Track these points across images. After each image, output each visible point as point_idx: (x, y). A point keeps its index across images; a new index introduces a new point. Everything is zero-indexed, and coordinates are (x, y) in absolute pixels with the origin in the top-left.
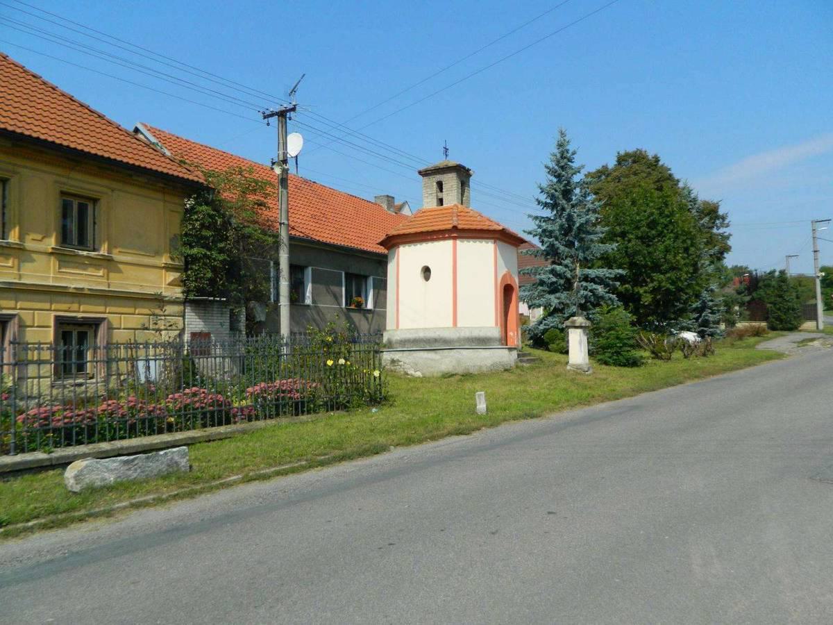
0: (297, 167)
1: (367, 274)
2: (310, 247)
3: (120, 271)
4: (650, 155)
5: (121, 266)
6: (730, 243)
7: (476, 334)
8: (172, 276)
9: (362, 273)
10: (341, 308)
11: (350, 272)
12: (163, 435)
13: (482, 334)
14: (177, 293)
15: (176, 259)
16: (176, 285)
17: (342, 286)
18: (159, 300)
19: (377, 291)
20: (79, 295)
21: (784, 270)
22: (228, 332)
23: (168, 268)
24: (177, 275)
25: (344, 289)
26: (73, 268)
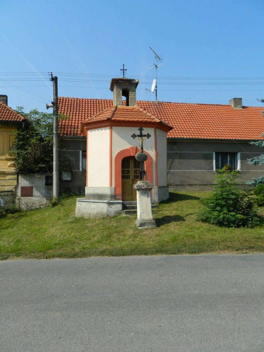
0: (156, 97)
1: (236, 151)
2: (208, 142)
7: (97, 192)
8: (9, 163)
12: (137, 211)
13: (100, 192)
14: (13, 170)
15: (13, 156)
16: (12, 167)
22: (44, 186)
23: (7, 160)
24: (13, 162)
25: (214, 161)
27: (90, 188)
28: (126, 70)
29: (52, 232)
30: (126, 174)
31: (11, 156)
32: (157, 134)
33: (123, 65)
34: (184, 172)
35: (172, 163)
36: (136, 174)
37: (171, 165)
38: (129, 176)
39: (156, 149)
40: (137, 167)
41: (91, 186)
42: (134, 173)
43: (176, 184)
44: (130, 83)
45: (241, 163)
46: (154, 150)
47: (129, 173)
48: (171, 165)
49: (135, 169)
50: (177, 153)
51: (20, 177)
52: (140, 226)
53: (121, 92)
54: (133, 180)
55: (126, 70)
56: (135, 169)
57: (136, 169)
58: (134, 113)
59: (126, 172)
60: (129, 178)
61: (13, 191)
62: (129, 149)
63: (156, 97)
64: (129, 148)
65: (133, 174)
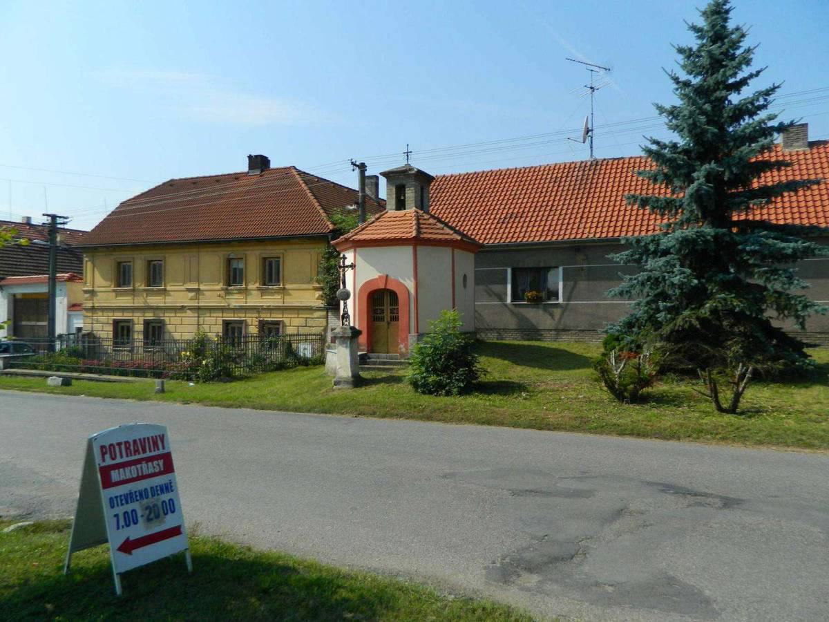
0: (592, 151)
3: (290, 295)
4: (39, 219)
5: (290, 291)
6: (689, 47)
9: (542, 265)
10: (506, 305)
11: (521, 265)
14: (320, 303)
17: (506, 283)
18: (310, 309)
19: (571, 283)
20: (270, 309)
21: (250, 157)
23: (316, 289)
24: (321, 293)
25: (509, 287)
26: (268, 295)
28: (411, 152)
31: (319, 284)
32: (418, 256)
33: (408, 145)
34: (597, 305)
35: (573, 289)
37: (571, 293)
39: (416, 277)
42: (391, 313)
43: (579, 329)
44: (405, 175)
46: (412, 279)
48: (571, 293)
49: (391, 307)
50: (582, 269)
51: (330, 314)
52: (335, 385)
53: (394, 190)
55: (411, 152)
56: (391, 307)
58: (406, 222)
59: (379, 311)
61: (321, 335)
62: (377, 279)
63: (592, 151)
64: (377, 277)
65: (389, 315)
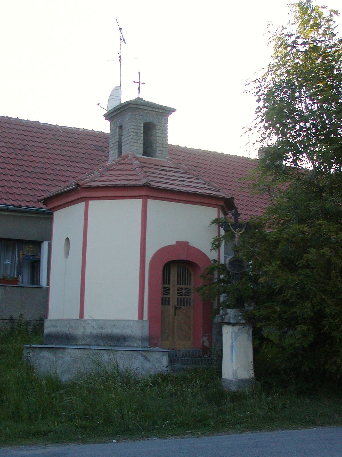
27: (89, 322)
29: (323, 306)
30: (184, 297)
33: (139, 73)
36: (181, 297)
38: (169, 298)
40: (183, 282)
41: (52, 319)
45: (225, 244)
47: (169, 293)
54: (176, 309)
55: (144, 83)
57: (181, 286)
60: (169, 304)
65: (177, 296)
